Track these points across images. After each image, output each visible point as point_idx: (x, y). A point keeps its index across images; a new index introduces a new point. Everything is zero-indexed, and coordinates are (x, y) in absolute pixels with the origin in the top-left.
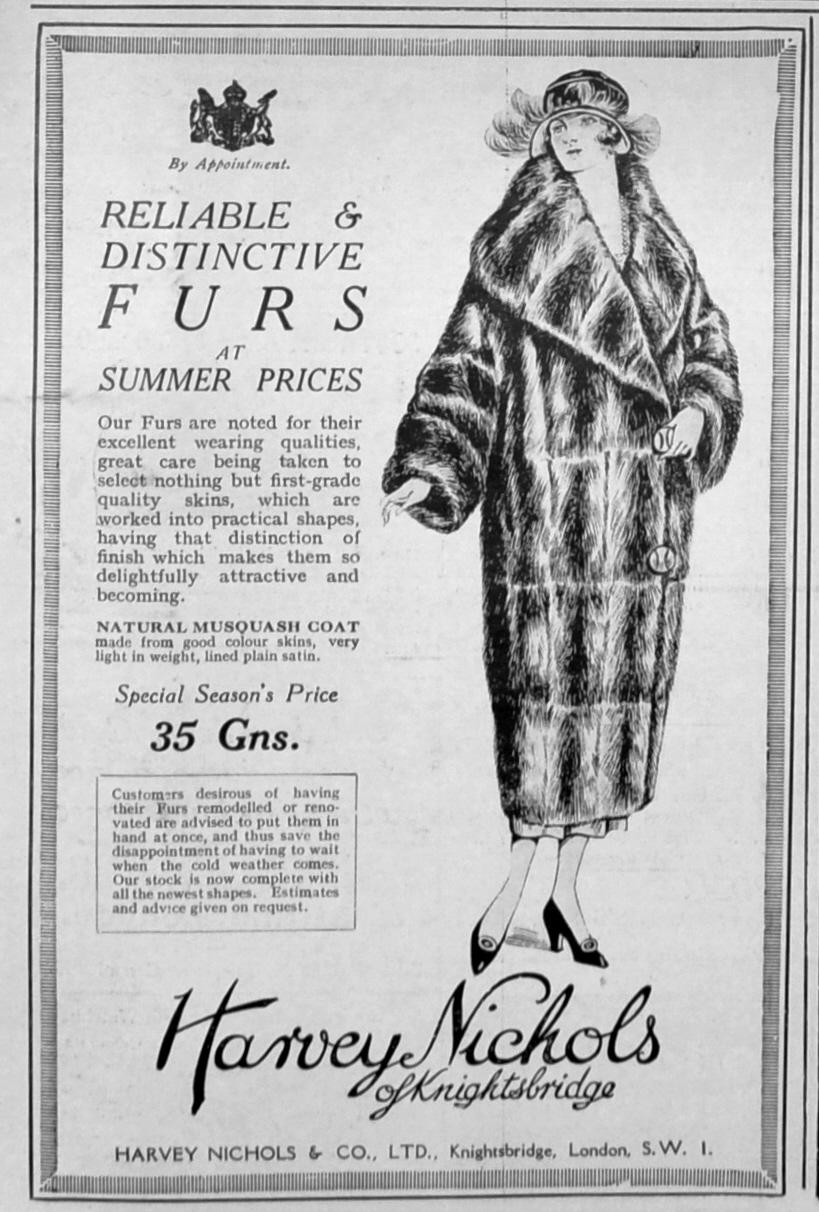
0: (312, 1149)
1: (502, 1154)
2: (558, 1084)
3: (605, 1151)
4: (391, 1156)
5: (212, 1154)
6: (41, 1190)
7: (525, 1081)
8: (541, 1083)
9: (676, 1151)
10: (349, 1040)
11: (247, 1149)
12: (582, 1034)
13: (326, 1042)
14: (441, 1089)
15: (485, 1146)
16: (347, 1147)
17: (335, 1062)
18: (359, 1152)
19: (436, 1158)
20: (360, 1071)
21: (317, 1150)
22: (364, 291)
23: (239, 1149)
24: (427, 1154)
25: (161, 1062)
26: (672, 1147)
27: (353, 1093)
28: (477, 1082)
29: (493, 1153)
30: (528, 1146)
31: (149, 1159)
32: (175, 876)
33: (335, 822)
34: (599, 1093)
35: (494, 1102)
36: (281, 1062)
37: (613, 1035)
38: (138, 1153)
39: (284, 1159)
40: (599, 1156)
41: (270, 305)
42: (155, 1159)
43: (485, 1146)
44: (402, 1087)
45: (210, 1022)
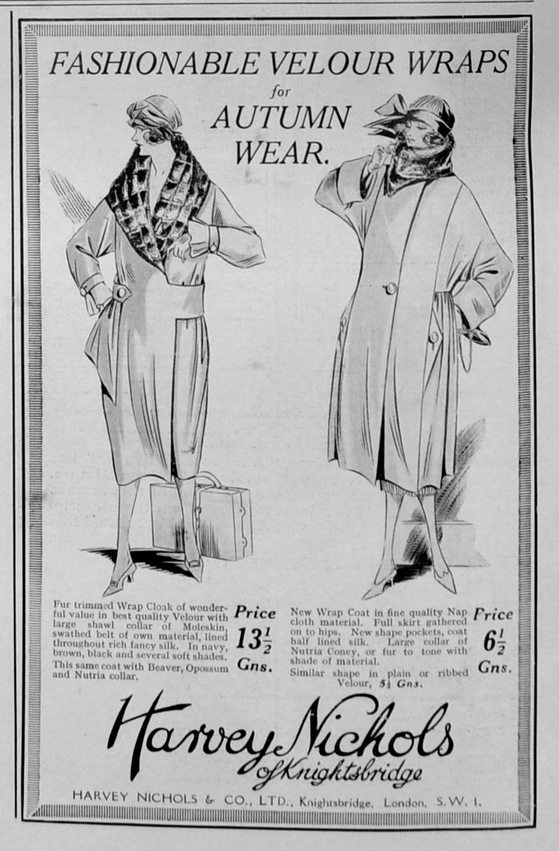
2: (383, 770)
4: (261, 804)
5: (140, 797)
7: (360, 768)
8: (371, 770)
9: (460, 804)
10: (238, 735)
13: (223, 736)
14: (302, 771)
17: (229, 750)
18: (239, 800)
20: (246, 757)
21: (211, 798)
23: (231, 797)
26: (457, 801)
27: (241, 771)
28: (327, 768)
29: (329, 804)
30: (354, 800)
31: (95, 798)
34: (412, 777)
35: (339, 781)
37: (422, 737)
39: (189, 803)
42: (100, 799)
44: (275, 769)
45: (143, 718)
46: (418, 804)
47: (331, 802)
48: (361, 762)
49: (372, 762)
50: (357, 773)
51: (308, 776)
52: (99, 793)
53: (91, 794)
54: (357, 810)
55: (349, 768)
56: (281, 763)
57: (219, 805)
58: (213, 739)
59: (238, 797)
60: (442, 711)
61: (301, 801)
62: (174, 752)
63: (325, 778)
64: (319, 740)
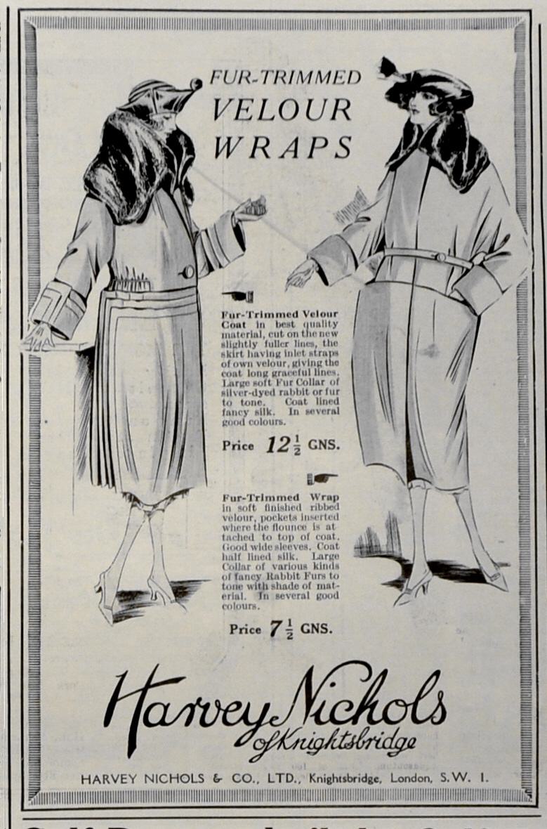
0: (215, 775)
1: (345, 781)
2: (377, 739)
3: (415, 779)
4: (269, 781)
5: (147, 779)
6: (29, 805)
7: (355, 736)
8: (365, 738)
9: (463, 780)
11: (171, 775)
12: (394, 704)
13: (219, 708)
14: (297, 742)
15: (333, 775)
16: (239, 775)
17: (225, 722)
19: (299, 783)
20: (242, 728)
21: (219, 777)
22: (350, 138)
23: (166, 775)
24: (294, 779)
25: (107, 722)
26: (460, 776)
27: (238, 744)
28: (323, 737)
31: (104, 783)
32: (279, 515)
34: (406, 746)
36: (188, 723)
37: (415, 704)
38: (97, 779)
39: (196, 782)
40: (411, 783)
42: (109, 782)
43: (333, 775)
44: (271, 740)
45: (140, 693)
47: (340, 778)
48: (356, 730)
50: (352, 742)
51: (303, 746)
52: (108, 777)
53: (100, 778)
55: (344, 737)
56: (277, 734)
59: (183, 775)
60: (434, 678)
61: (311, 778)
64: (314, 710)
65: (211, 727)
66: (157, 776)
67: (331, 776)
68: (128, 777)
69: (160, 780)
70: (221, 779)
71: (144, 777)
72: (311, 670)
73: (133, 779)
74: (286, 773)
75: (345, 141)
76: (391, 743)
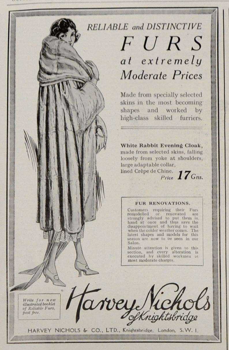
0: (84, 329)
2: (181, 316)
4: (107, 332)
7: (172, 315)
8: (176, 316)
9: (189, 331)
12: (188, 301)
14: (147, 317)
17: (117, 308)
18: (98, 330)
20: (124, 311)
22: (201, 37)
23: (64, 329)
27: (122, 317)
28: (158, 315)
29: (135, 331)
31: (37, 332)
33: (197, 219)
34: (193, 319)
37: (197, 302)
38: (34, 330)
39: (77, 332)
41: (172, 42)
42: (39, 332)
44: (136, 316)
45: (81, 296)
46: (172, 331)
47: (136, 330)
48: (172, 312)
49: (177, 312)
50: (170, 317)
51: (150, 319)
54: (147, 333)
55: (167, 315)
56: (139, 313)
57: (89, 332)
58: (110, 304)
59: (73, 332)
60: (205, 290)
61: (124, 330)
62: (94, 310)
63: (157, 319)
65: (119, 310)
66: (60, 329)
67: (132, 329)
68: (48, 329)
69: (73, 329)
70: (87, 331)
71: (55, 330)
72: (153, 287)
73: (49, 331)
74: (114, 328)
75: (198, 39)
76: (187, 318)
